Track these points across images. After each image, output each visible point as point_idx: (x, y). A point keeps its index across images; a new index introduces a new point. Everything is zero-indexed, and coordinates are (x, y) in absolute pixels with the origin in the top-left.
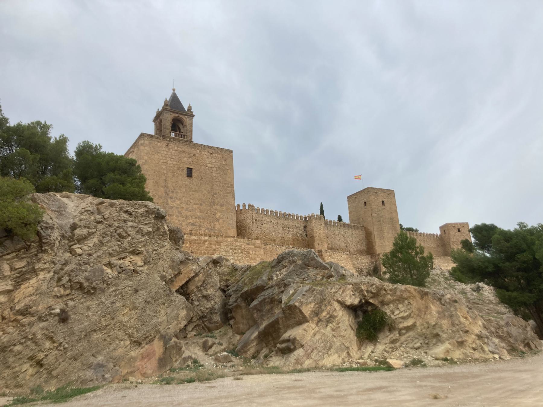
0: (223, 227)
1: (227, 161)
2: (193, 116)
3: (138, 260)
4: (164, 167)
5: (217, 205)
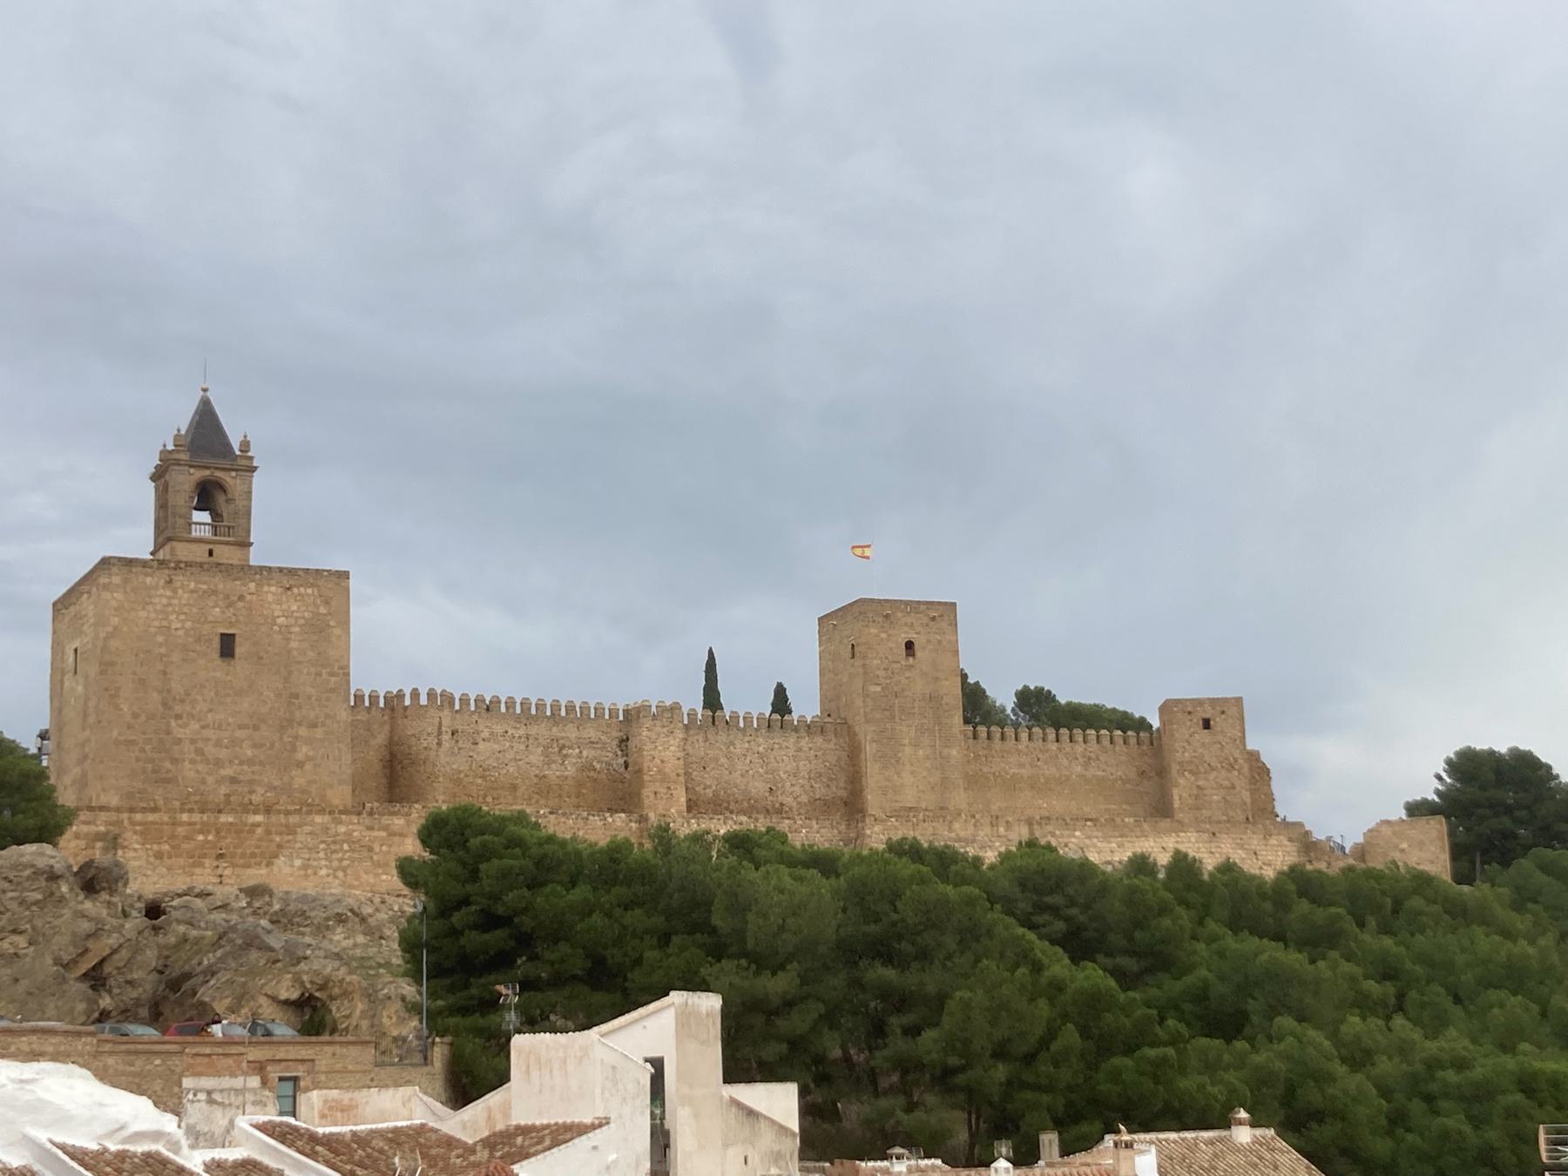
0: (314, 782)
1: (333, 603)
2: (254, 469)
3: (21, 941)
4: (160, 639)
5: (300, 724)
